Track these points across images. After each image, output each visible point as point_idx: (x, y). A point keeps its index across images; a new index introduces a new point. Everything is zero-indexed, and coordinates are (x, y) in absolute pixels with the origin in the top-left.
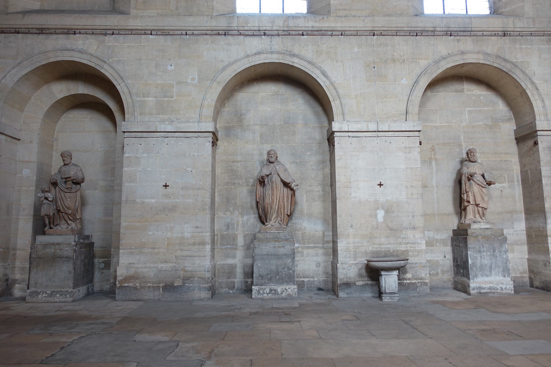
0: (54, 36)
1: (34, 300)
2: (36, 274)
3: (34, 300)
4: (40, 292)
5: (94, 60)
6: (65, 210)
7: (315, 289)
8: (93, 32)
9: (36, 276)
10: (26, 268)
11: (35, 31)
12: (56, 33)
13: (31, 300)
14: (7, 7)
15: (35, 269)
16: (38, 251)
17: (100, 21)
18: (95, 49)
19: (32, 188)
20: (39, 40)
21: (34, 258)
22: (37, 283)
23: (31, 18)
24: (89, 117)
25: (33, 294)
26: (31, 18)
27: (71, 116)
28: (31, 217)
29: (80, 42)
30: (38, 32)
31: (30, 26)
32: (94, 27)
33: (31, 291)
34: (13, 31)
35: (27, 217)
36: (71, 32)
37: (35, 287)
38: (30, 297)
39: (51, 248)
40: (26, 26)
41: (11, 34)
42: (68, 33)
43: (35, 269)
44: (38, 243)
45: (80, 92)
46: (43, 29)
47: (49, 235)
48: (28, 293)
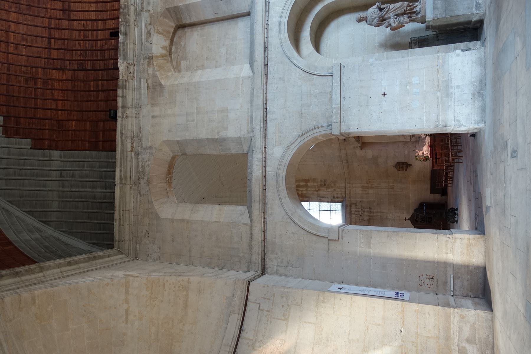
0: (270, 39)
1: (483, 6)
2: (460, 10)
3: (483, 6)
4: (476, 2)
5: (287, 6)
6: (404, 7)
7: (484, 18)
8: (267, 12)
9: (462, 10)
10: (454, 46)
11: (266, 53)
12: (268, 38)
13: (483, 8)
14: (249, 77)
15: (456, 12)
16: (440, 13)
17: (259, 29)
18: (279, 8)
19: (385, 56)
20: (272, 49)
21: (446, 15)
22: (468, 7)
23: (257, 56)
24: (327, 41)
25: (478, 8)
26: (257, 56)
27: (326, 55)
28: (410, 51)
29: (274, 20)
30: (266, 51)
31: (263, 55)
32: (264, 10)
33: (475, 9)
34: (266, 68)
35: (410, 54)
36: (267, 27)
37: (472, 8)
38: (481, 10)
39: (437, 3)
40: (263, 58)
41: (268, 70)
42: (268, 29)
43: (456, 12)
44: (433, 14)
45: (309, 33)
46: (265, 47)
47: (425, 13)
48: (477, 11)
